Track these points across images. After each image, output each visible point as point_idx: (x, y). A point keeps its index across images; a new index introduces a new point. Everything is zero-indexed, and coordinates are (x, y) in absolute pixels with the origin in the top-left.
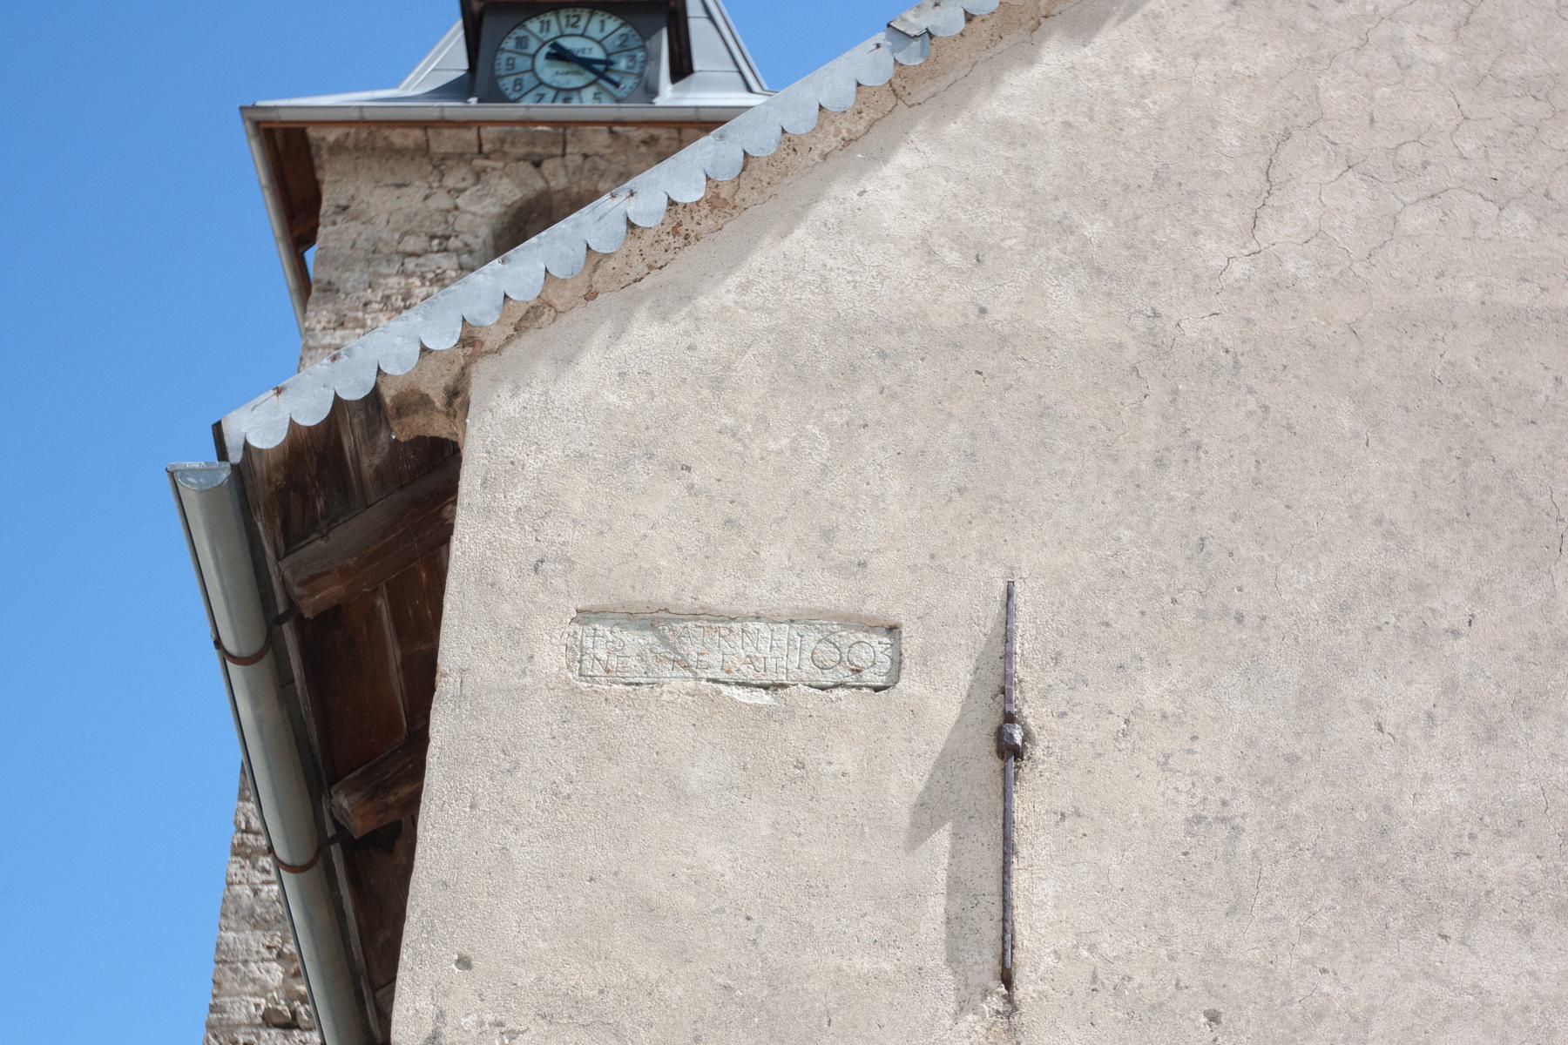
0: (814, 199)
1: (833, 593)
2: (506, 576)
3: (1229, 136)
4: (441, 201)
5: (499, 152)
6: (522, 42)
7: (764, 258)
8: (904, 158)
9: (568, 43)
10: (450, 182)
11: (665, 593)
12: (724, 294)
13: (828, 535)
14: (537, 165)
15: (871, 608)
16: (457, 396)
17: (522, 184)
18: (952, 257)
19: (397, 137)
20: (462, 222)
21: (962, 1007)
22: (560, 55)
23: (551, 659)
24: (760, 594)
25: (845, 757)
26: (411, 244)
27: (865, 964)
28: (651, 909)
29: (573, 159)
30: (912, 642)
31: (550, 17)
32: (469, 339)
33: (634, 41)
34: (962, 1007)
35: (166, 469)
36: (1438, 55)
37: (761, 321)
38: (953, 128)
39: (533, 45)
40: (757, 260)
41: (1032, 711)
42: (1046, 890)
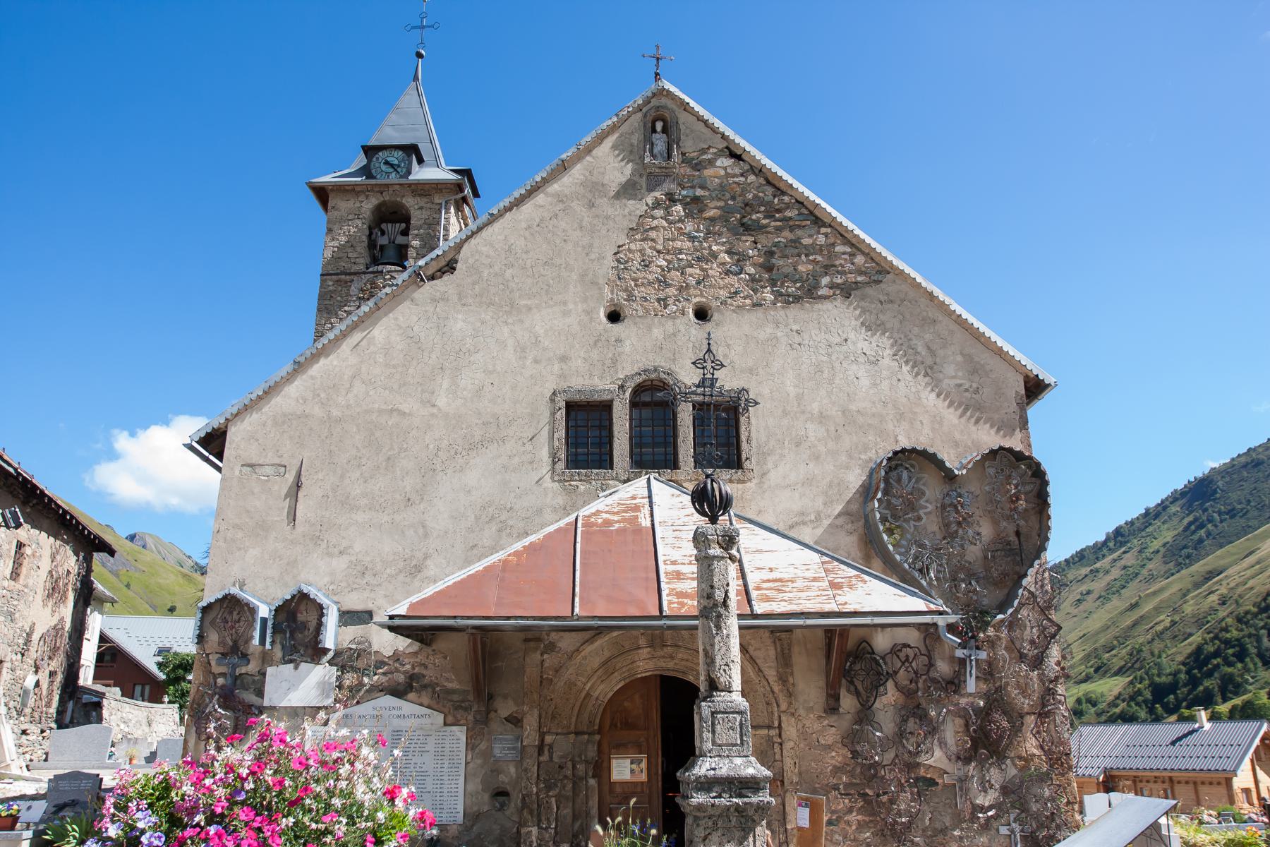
0: (281, 391)
1: (277, 461)
2: (231, 459)
3: (346, 377)
4: (358, 205)
5: (372, 190)
6: (377, 158)
7: (273, 402)
8: (296, 383)
9: (389, 159)
10: (360, 199)
11: (254, 462)
12: (266, 409)
13: (278, 451)
14: (382, 193)
15: (283, 463)
16: (226, 427)
17: (378, 199)
18: (301, 401)
19: (347, 187)
20: (363, 210)
21: (288, 525)
22: (387, 163)
23: (237, 473)
24: (268, 462)
25: (276, 487)
26: (351, 217)
27: (276, 519)
28: (248, 511)
29: (391, 192)
30: (288, 469)
31: (385, 151)
32: (227, 419)
33: (406, 158)
34: (288, 525)
35: (112, 552)
36: (381, 360)
37: (271, 414)
38: (304, 377)
39: (380, 159)
40: (272, 403)
41: (303, 479)
42: (301, 507)
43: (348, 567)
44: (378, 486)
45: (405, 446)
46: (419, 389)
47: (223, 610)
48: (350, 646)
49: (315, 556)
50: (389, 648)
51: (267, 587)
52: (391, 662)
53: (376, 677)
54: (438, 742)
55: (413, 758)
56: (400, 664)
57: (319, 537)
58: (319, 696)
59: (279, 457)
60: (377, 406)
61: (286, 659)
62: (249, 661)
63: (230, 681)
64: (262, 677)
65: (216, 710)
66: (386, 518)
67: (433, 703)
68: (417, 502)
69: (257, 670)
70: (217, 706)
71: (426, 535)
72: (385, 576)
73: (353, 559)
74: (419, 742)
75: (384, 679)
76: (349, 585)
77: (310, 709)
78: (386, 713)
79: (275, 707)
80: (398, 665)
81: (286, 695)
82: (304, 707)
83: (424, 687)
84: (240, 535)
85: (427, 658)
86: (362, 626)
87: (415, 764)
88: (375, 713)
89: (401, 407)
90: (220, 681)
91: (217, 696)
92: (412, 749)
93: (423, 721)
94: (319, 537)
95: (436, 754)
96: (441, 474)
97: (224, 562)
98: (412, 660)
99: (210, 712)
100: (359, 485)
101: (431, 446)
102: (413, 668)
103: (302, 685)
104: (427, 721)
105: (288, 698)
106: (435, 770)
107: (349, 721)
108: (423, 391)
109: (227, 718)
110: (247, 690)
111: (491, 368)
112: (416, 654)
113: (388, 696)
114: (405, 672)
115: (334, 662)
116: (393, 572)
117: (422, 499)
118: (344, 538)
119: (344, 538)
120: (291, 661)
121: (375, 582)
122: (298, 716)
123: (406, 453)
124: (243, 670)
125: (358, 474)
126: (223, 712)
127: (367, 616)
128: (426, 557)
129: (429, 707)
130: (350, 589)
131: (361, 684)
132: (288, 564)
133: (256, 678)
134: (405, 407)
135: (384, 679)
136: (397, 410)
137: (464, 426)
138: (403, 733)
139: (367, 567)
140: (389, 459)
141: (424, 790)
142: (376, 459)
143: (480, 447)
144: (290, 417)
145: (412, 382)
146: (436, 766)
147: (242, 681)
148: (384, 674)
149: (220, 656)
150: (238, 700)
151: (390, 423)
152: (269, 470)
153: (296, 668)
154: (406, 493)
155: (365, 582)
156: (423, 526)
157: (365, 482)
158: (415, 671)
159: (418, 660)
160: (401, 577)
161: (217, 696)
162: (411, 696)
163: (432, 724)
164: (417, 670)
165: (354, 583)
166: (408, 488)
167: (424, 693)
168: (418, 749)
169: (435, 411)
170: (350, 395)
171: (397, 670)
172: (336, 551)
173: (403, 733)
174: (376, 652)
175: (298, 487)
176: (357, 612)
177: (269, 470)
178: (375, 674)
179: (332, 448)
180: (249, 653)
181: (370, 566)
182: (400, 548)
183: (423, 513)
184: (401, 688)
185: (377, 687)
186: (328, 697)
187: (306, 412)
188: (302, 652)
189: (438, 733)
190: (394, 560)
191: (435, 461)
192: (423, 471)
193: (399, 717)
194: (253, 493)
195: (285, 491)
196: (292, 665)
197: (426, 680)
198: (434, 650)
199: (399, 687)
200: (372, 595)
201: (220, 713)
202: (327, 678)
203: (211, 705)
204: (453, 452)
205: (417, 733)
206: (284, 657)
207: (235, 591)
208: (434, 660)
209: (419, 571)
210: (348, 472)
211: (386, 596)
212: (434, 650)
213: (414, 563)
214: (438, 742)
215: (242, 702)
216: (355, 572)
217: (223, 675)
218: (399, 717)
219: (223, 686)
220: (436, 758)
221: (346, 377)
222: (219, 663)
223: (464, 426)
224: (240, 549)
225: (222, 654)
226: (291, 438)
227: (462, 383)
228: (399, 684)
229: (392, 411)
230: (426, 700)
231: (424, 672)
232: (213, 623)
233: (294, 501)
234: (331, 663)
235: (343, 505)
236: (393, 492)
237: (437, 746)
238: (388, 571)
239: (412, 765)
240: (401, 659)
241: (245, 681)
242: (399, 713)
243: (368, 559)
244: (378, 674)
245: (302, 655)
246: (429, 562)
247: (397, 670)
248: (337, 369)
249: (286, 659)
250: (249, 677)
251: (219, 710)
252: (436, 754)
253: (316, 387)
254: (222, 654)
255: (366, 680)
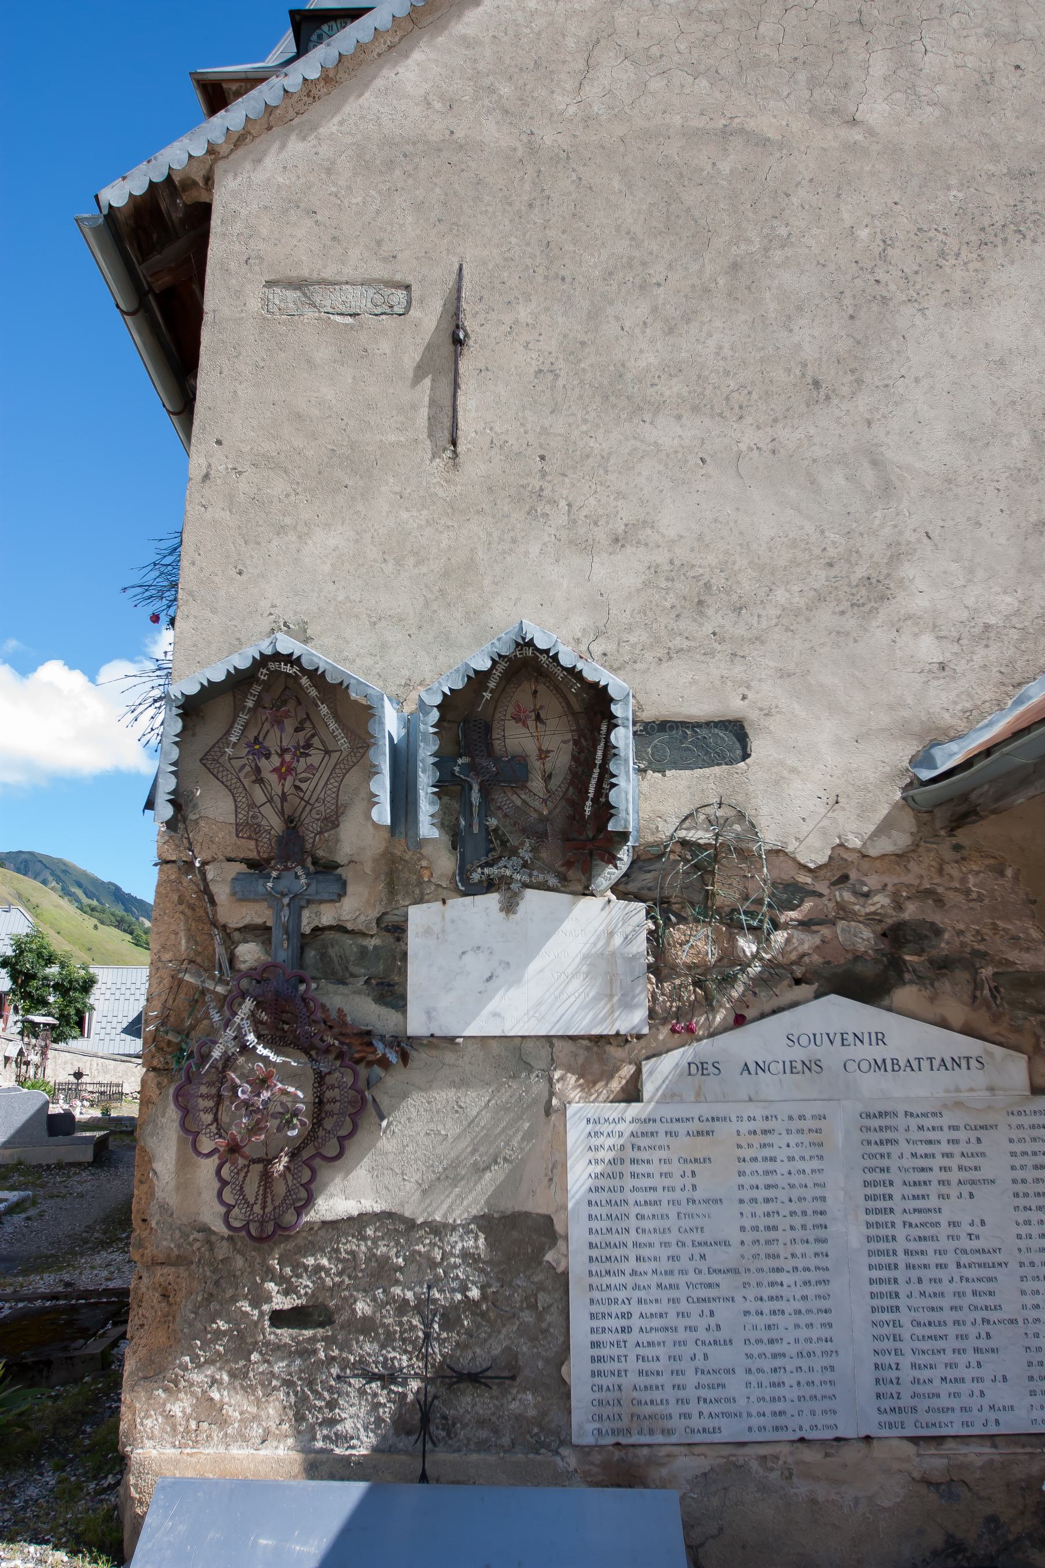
1: (380, 271)
2: (233, 266)
3: (571, 43)
8: (417, 56)
11: (305, 273)
12: (331, 127)
13: (379, 243)
15: (398, 277)
18: (438, 106)
23: (254, 305)
24: (348, 272)
25: (385, 346)
27: (392, 438)
28: (299, 417)
30: (416, 292)
31: (332, 23)
37: (349, 140)
40: (347, 109)
41: (469, 323)
42: (472, 404)
43: (646, 584)
44: (711, 343)
45: (783, 231)
46: (802, 76)
47: (244, 717)
48: (682, 834)
49: (534, 549)
50: (814, 841)
51: (384, 646)
52: (822, 887)
53: (779, 937)
54: (1018, 1148)
55: (944, 1205)
56: (856, 893)
57: (540, 494)
58: (596, 999)
59: (385, 260)
60: (678, 120)
61: (476, 877)
62: (341, 894)
63: (283, 953)
64: (390, 939)
65: (244, 1049)
66: (749, 437)
67: (981, 1019)
68: (845, 390)
69: (375, 914)
70: (251, 1038)
71: (887, 489)
72: (774, 612)
73: (661, 557)
74: (955, 1149)
75: (807, 942)
76: (657, 640)
77: (569, 1046)
78: (832, 1056)
79: (451, 1040)
80: (848, 896)
81: (483, 996)
82: (549, 1039)
83: (943, 966)
84: (279, 486)
85: (941, 871)
86: (716, 770)
87: (953, 1224)
88: (797, 1054)
89: (751, 124)
90: (249, 953)
91: (248, 1004)
92: (935, 1176)
93: (961, 1078)
94: (540, 494)
95: (1020, 1188)
96: (908, 310)
97: (233, 572)
98: (891, 880)
99: (228, 1061)
100: (652, 341)
101: (863, 234)
102: (899, 907)
103: (534, 966)
104: (972, 1079)
105: (491, 1007)
106: (1022, 1244)
107: (711, 1083)
108: (813, 83)
109: (290, 1077)
110: (342, 982)
111: (1005, 24)
112: (900, 858)
113: (833, 997)
114: (872, 919)
115: (632, 887)
116: (800, 601)
117: (859, 381)
118: (620, 495)
119: (620, 495)
120: (489, 886)
121: (741, 631)
122: (529, 1068)
123: (789, 251)
124: (327, 916)
125: (643, 310)
126: (273, 1057)
127: (727, 738)
128: (897, 554)
129: (968, 1031)
130: (661, 652)
131: (731, 960)
132: (446, 574)
133: (371, 943)
134: (766, 124)
135: (807, 942)
136: (742, 131)
137: (953, 181)
138: (901, 1121)
139: (708, 586)
140: (735, 266)
141: (994, 1316)
142: (695, 267)
143: (1014, 239)
144: (409, 148)
145: (775, 57)
146: (1023, 1230)
147: (324, 956)
148: (805, 925)
149: (243, 867)
150: (319, 1015)
151: (725, 167)
152: (356, 298)
153: (509, 907)
154: (805, 365)
155: (708, 628)
156: (874, 463)
157: (671, 331)
158: (906, 916)
159: (909, 879)
160: (825, 617)
161: (248, 1004)
162: (905, 995)
163: (991, 1089)
164: (911, 911)
165: (672, 633)
166: (809, 352)
167: (945, 985)
168: (955, 1176)
169: (856, 135)
170: (591, 91)
171: (844, 912)
172: (601, 535)
173: (901, 1121)
174: (777, 852)
175: (458, 342)
176: (695, 726)
177: (356, 298)
178: (776, 926)
179: (552, 234)
180: (341, 859)
181: (718, 581)
182: (809, 528)
183: (869, 423)
184: (868, 970)
185: (788, 967)
186: (627, 1004)
187: (460, 134)
188: (525, 854)
189: (1016, 1120)
190: (794, 562)
191: (880, 275)
192: (847, 301)
193: (880, 1065)
194: (311, 363)
195: (412, 356)
196: (492, 900)
197: (944, 947)
198: (957, 848)
199: (859, 968)
200: (738, 670)
201: (265, 1059)
202: (618, 940)
203: (230, 1033)
204: (931, 249)
205: (945, 1121)
206: (463, 872)
207: (286, 645)
208: (964, 880)
209: (883, 598)
210: (611, 303)
211: (783, 674)
212: (957, 848)
213: (860, 572)
214: (1018, 1148)
215: (337, 1024)
216: (671, 599)
217: (260, 932)
218: (880, 1065)
219: (260, 975)
220: (1021, 1202)
221: (571, 43)
222: (241, 895)
223: (953, 181)
224: (281, 530)
225: (251, 864)
226: (418, 207)
227: (930, 63)
228: (858, 958)
229: (725, 134)
230: (956, 1011)
231: (937, 918)
232: (210, 760)
233: (446, 383)
234: (622, 891)
235: (606, 398)
236: (762, 360)
237: (1018, 1162)
238: (781, 595)
239: (944, 1231)
240: (853, 875)
241: (332, 952)
242: (877, 1052)
243: (711, 559)
244: (786, 926)
245: (525, 865)
246: (907, 570)
247: (844, 912)
248: (540, 22)
249: (476, 877)
250: (347, 940)
251: (261, 1050)
252: (1020, 1188)
253: (481, 66)
254: (251, 864)
255: (747, 946)
